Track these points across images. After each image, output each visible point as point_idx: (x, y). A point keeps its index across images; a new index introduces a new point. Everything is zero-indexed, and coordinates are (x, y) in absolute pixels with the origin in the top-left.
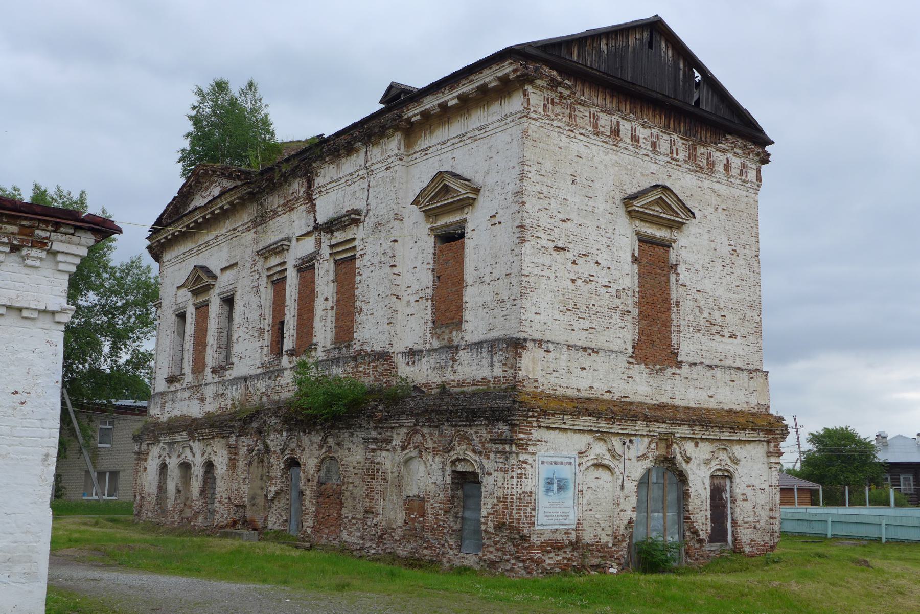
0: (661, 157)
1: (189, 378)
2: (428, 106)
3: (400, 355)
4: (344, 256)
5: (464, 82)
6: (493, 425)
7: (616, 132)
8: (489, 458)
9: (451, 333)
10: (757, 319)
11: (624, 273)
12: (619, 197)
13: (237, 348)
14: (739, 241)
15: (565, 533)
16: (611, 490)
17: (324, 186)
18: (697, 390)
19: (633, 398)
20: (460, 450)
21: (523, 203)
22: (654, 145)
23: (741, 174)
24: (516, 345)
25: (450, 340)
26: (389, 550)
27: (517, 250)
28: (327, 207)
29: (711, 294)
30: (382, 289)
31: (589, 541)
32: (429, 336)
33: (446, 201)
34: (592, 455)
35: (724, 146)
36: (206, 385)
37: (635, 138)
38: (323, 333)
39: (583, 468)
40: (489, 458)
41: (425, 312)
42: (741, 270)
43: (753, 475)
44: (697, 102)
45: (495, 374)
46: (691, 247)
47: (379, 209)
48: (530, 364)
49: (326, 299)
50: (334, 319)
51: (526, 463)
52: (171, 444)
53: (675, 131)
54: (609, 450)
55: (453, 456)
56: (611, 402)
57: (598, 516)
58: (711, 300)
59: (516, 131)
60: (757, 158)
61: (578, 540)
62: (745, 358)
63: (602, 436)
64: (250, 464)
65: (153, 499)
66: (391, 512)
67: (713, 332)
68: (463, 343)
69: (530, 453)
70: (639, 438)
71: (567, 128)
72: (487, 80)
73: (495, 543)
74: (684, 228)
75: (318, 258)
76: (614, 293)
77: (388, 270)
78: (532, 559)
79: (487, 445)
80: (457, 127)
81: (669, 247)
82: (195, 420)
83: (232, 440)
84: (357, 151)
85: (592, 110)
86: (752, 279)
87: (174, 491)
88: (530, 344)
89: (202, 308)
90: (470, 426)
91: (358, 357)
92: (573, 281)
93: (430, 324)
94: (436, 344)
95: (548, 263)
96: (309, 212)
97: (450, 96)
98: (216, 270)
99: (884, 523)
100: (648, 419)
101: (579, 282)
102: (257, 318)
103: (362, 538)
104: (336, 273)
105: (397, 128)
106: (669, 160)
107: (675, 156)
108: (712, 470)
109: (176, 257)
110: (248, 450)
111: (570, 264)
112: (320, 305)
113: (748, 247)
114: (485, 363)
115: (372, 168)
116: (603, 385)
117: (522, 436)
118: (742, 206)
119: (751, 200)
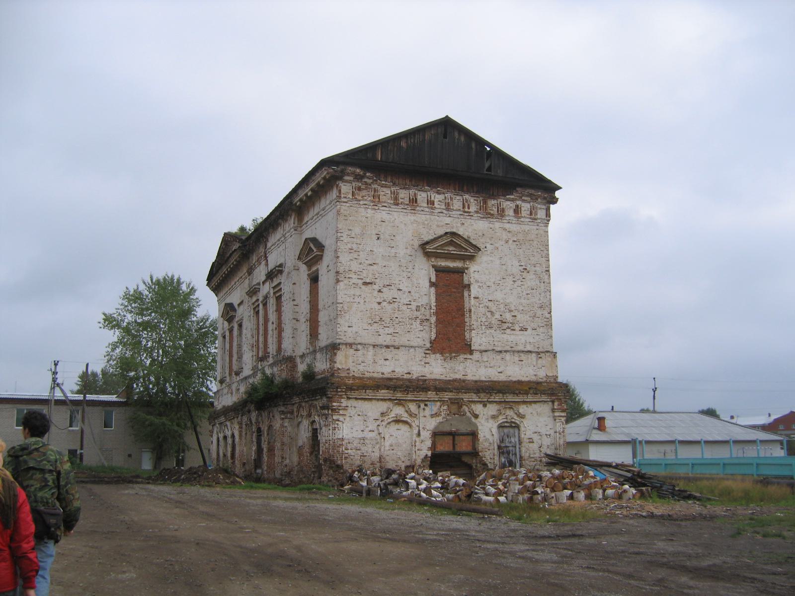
0: (454, 212)
12: (417, 243)
14: (530, 262)
18: (487, 369)
19: (429, 376)
23: (531, 214)
29: (502, 301)
39: (384, 423)
44: (489, 169)
51: (338, 420)
54: (407, 411)
56: (410, 380)
57: (399, 453)
58: (502, 306)
62: (536, 344)
63: (400, 402)
67: (505, 328)
71: (372, 204)
81: (463, 273)
85: (392, 189)
86: (542, 288)
92: (379, 303)
100: (438, 390)
101: (384, 304)
107: (466, 210)
111: (376, 292)
113: (538, 265)
116: (403, 370)
119: (542, 232)
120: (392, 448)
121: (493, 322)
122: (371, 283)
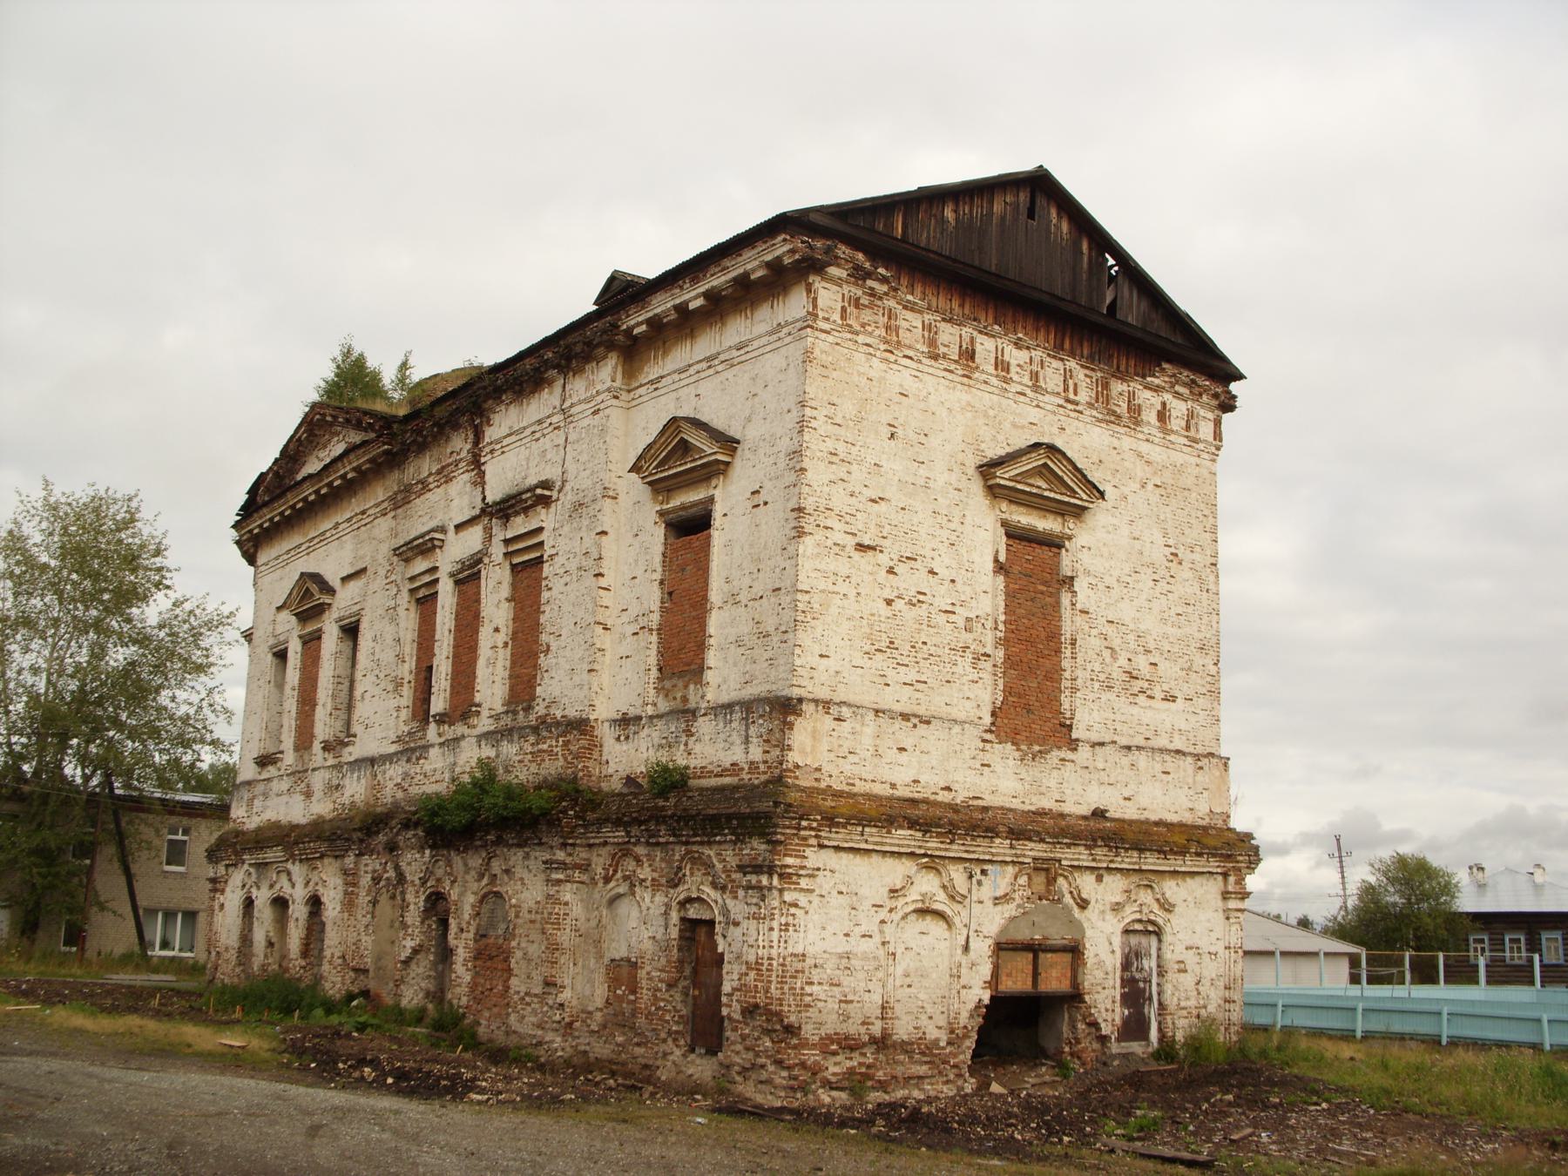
0: (1047, 398)
1: (289, 758)
2: (658, 310)
3: (607, 725)
4: (526, 557)
5: (713, 269)
6: (743, 842)
7: (969, 355)
8: (736, 898)
9: (686, 687)
10: (1213, 670)
11: (979, 590)
12: (972, 461)
13: (362, 710)
15: (863, 1023)
16: (947, 952)
17: (498, 441)
19: (990, 800)
20: (695, 884)
21: (803, 470)
22: (1035, 376)
23: (1188, 428)
24: (785, 708)
25: (685, 700)
26: (582, 1048)
27: (791, 549)
28: (503, 475)
29: (1132, 626)
30: (581, 614)
31: (905, 1037)
32: (652, 692)
33: (685, 465)
34: (913, 895)
35: (1157, 381)
36: (314, 770)
37: (1002, 365)
38: (491, 688)
39: (896, 917)
40: (736, 898)
41: (649, 653)
42: (1186, 584)
43: (1198, 929)
44: (1112, 307)
45: (751, 757)
46: (1096, 548)
47: (580, 480)
48: (809, 742)
49: (497, 630)
50: (508, 664)
51: (796, 905)
52: (262, 866)
53: (1072, 354)
54: (944, 887)
55: (681, 893)
57: (922, 996)
58: (1132, 637)
59: (795, 351)
60: (1215, 402)
61: (886, 1036)
63: (933, 863)
64: (374, 903)
65: (232, 956)
66: (583, 987)
67: (1136, 690)
68: (704, 705)
69: (802, 890)
70: (997, 868)
71: (883, 347)
72: (749, 267)
73: (744, 1037)
74: (1087, 516)
75: (486, 560)
76: (961, 623)
77: (590, 581)
78: (803, 1065)
79: (734, 876)
80: (706, 344)
81: (1060, 547)
82: (294, 827)
83: (350, 861)
84: (550, 383)
85: (927, 317)
86: (1205, 603)
87: (263, 943)
88: (808, 708)
89: (312, 642)
90: (709, 843)
91: (544, 726)
92: (889, 602)
93: (654, 673)
94: (663, 706)
95: (844, 571)
96: (475, 484)
97: (693, 294)
98: (333, 579)
99: (1445, 1011)
100: (1017, 834)
101: (899, 605)
102: (392, 659)
103: (540, 1026)
104: (514, 586)
105: (611, 346)
106: (1061, 402)
107: (1071, 396)
108: (1127, 921)
109: (277, 558)
110: (373, 879)
111: (883, 573)
112: (486, 638)
113: (1198, 549)
114: (737, 739)
115: (573, 411)
116: (936, 779)
117: (789, 861)
118: (1189, 481)
119: (1205, 472)
120: (908, 981)
121: (1114, 675)
122: (873, 548)
